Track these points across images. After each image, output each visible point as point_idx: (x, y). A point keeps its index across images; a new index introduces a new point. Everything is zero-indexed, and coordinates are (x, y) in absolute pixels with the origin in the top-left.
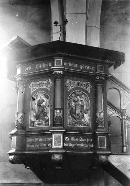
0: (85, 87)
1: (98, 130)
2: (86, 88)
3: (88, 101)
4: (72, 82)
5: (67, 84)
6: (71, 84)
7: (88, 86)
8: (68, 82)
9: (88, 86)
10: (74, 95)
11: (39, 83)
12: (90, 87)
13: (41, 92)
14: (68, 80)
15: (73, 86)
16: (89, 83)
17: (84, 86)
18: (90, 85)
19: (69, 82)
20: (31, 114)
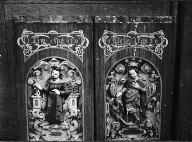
0: (151, 46)
1: (77, 96)
2: (154, 49)
3: (102, 82)
4: (115, 35)
5: (102, 44)
6: (112, 42)
7: (160, 41)
8: (104, 38)
9: (160, 41)
10: (121, 69)
11: (50, 35)
12: (164, 43)
13: (76, 83)
14: (105, 33)
15: (120, 47)
16: (161, 32)
17: (148, 44)
18: (164, 38)
19: (107, 37)
20: (107, 4)
